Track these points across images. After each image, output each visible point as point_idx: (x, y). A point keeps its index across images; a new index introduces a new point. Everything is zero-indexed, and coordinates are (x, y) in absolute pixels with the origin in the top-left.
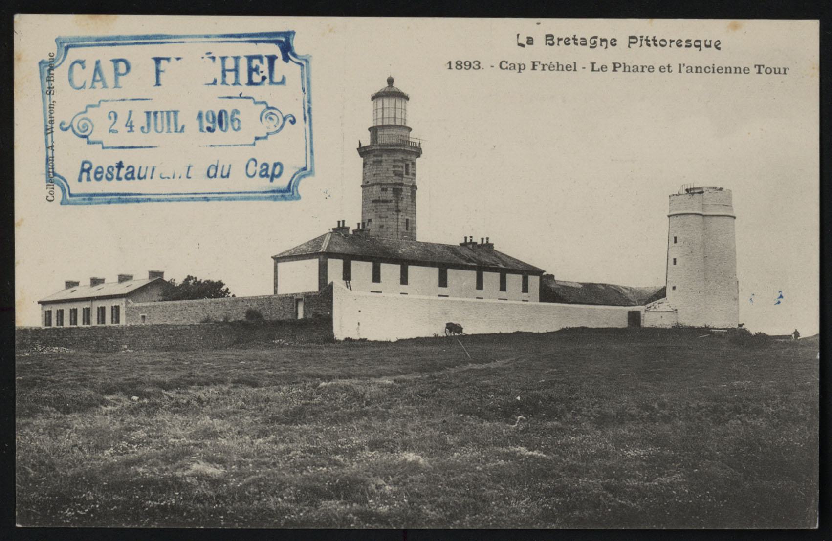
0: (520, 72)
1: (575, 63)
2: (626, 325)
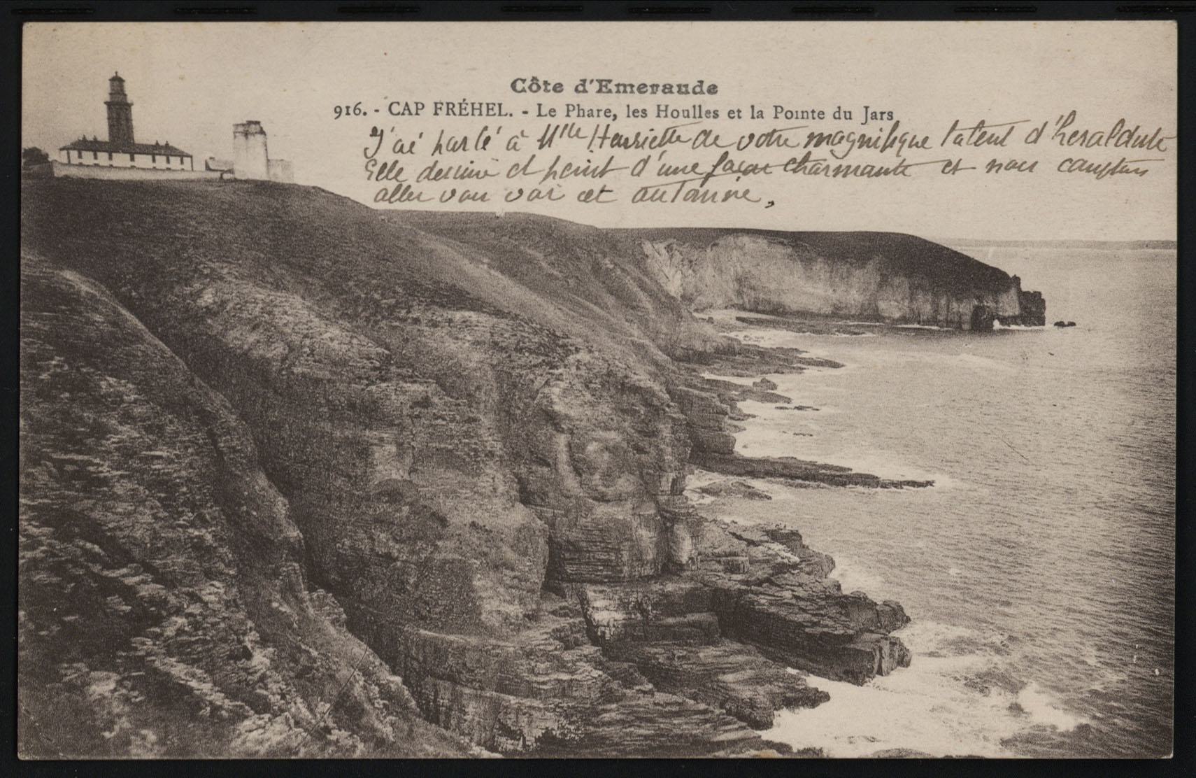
2: (35, 35)
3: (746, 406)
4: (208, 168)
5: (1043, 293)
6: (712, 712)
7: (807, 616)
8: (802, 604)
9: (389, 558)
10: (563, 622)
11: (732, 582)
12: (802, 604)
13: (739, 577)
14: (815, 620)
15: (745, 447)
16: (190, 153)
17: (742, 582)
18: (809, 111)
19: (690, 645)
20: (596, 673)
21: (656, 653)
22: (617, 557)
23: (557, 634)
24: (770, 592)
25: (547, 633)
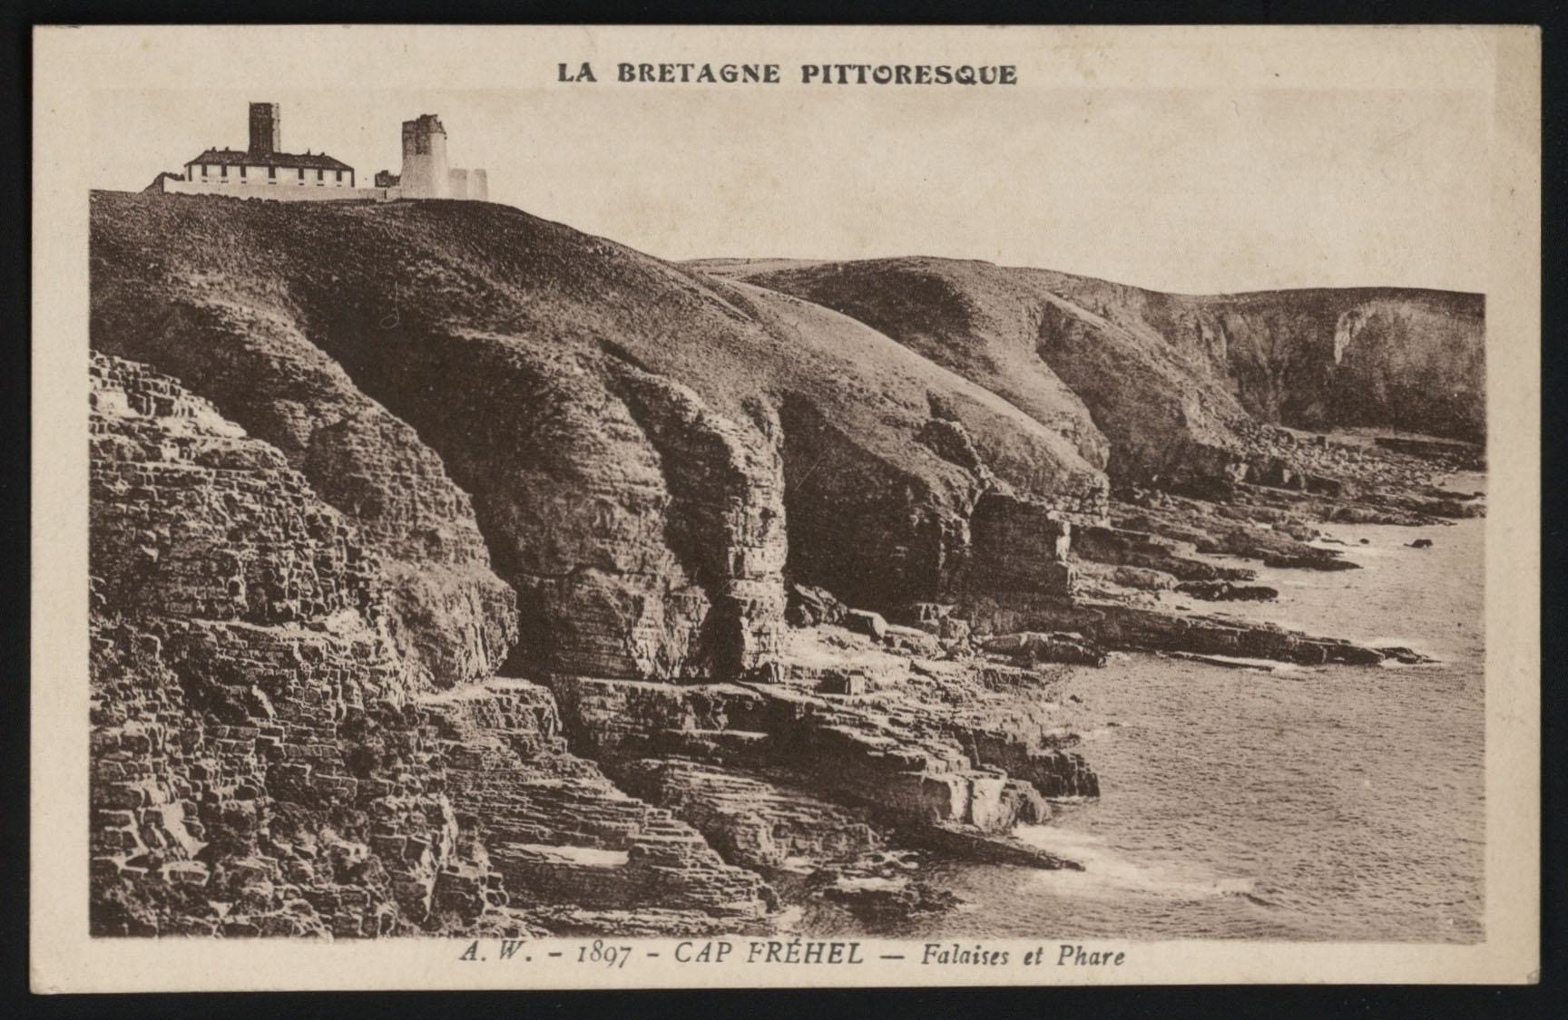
2: (50, 42)
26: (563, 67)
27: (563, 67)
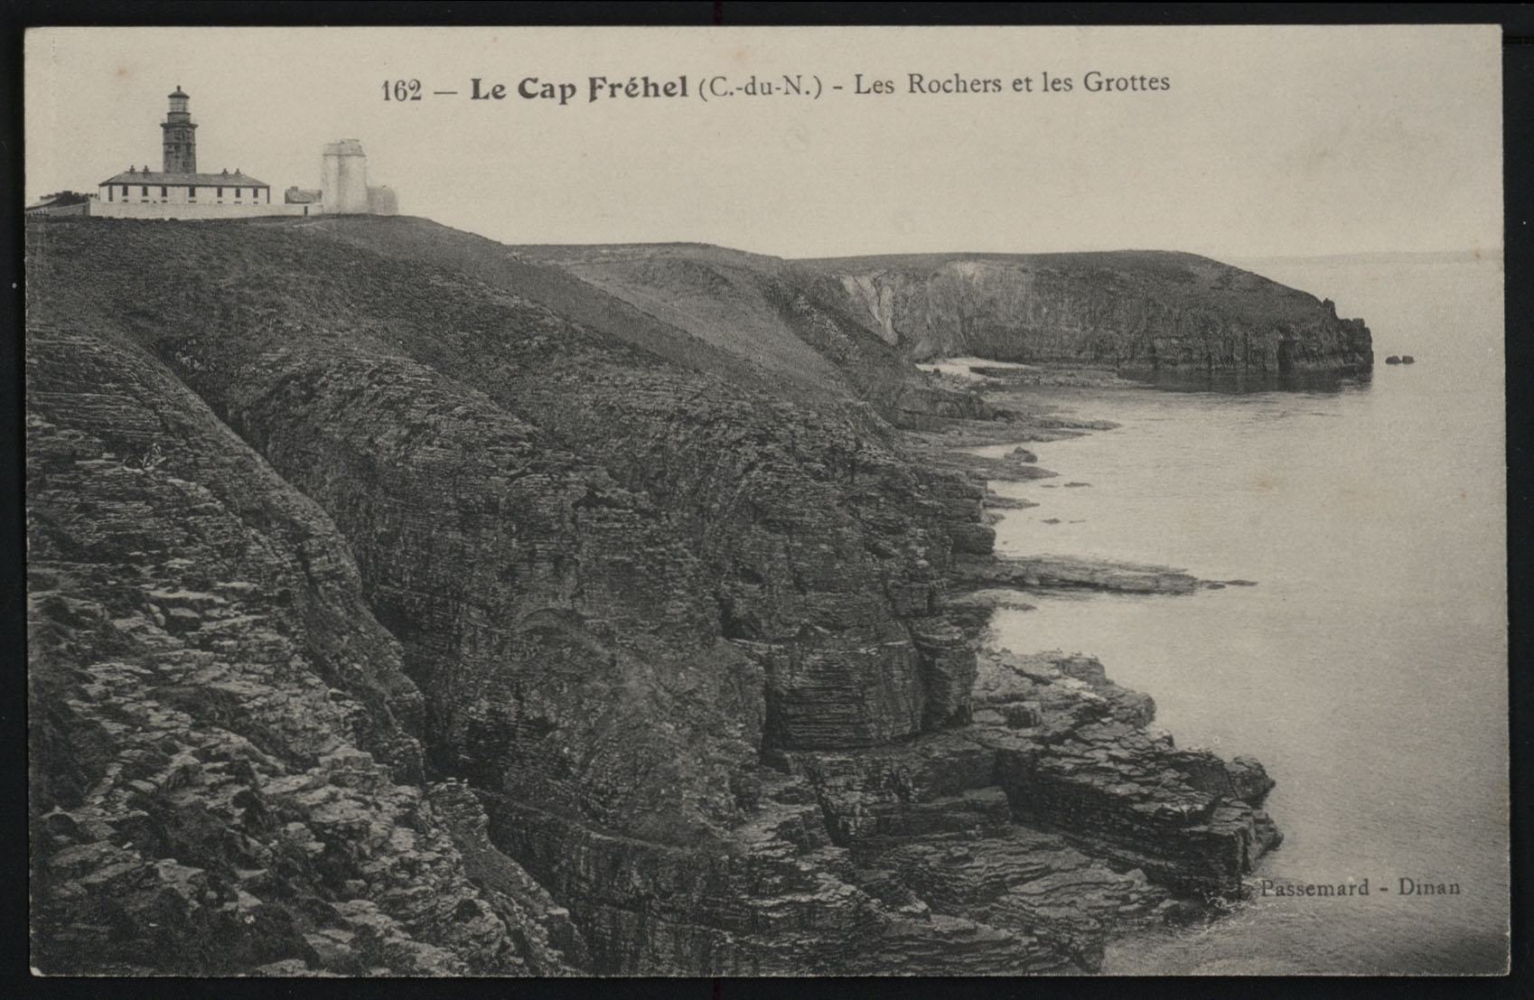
0: (563, 102)
1: (683, 79)
2: (39, 41)
3: (998, 488)
4: (288, 200)
5: (1365, 321)
6: (1018, 942)
7: (1134, 787)
8: (1124, 768)
9: (543, 726)
10: (794, 811)
11: (1020, 742)
12: (1124, 768)
13: (1029, 732)
14: (1145, 791)
15: (1005, 543)
16: (266, 182)
17: (1035, 739)
18: (1128, 78)
19: (973, 839)
20: (848, 889)
21: (925, 853)
22: (859, 709)
23: (785, 831)
24: (1076, 752)
25: (773, 830)
26: (476, 83)
27: (476, 83)
